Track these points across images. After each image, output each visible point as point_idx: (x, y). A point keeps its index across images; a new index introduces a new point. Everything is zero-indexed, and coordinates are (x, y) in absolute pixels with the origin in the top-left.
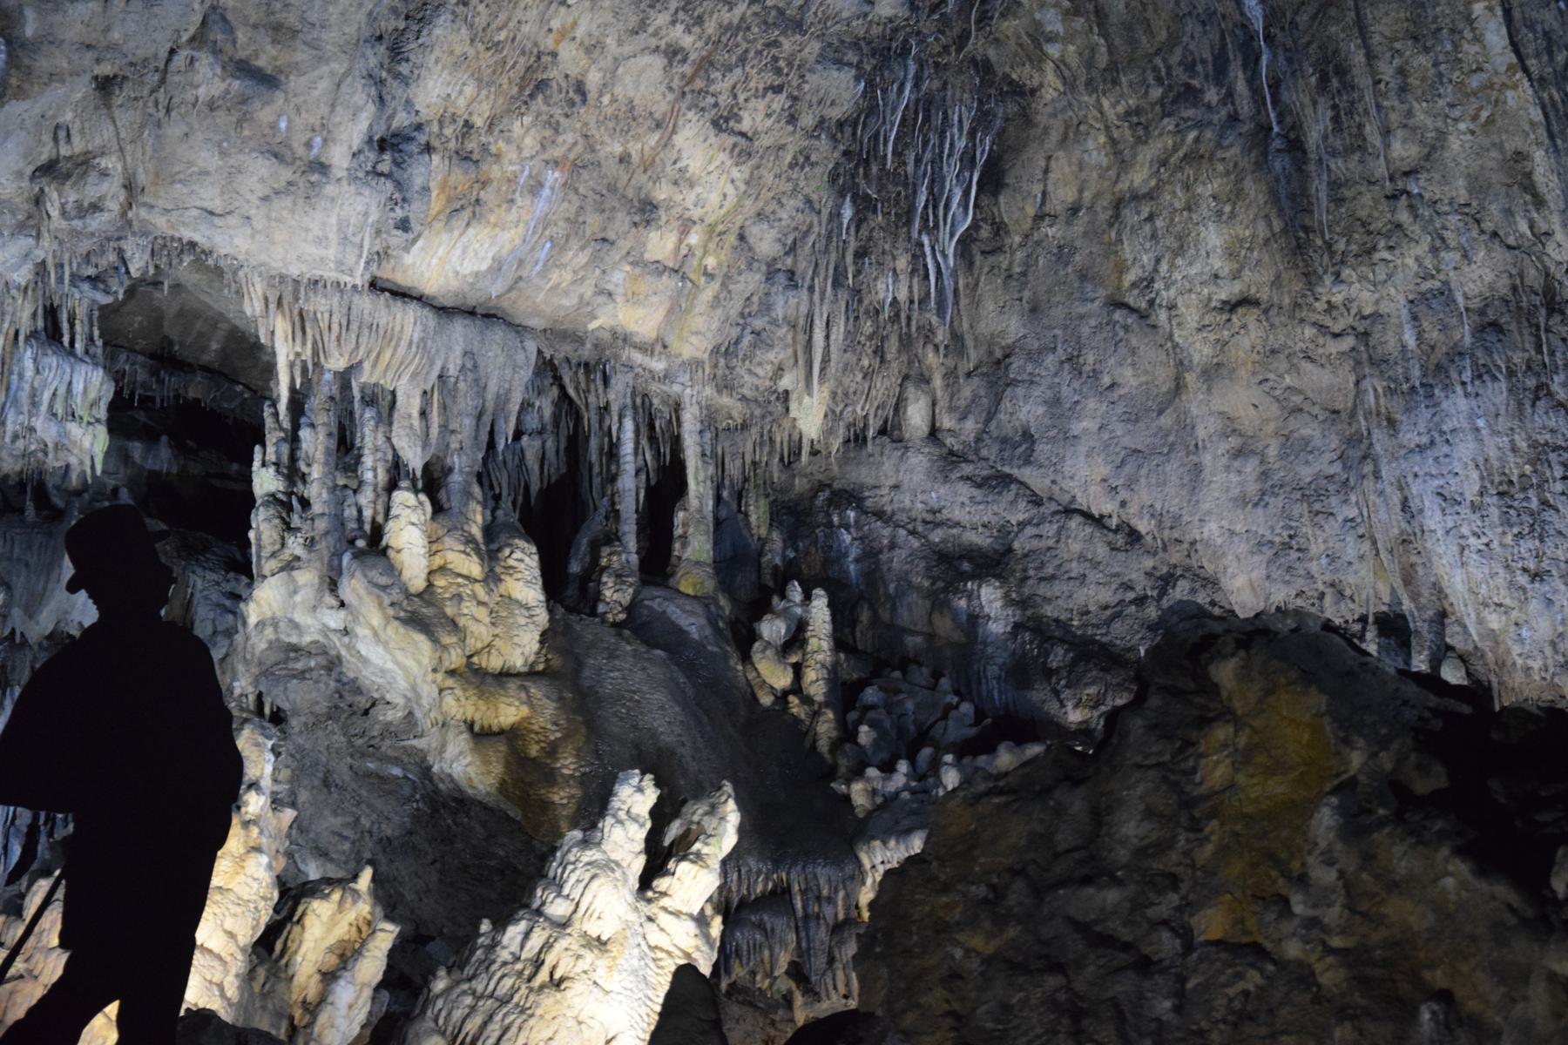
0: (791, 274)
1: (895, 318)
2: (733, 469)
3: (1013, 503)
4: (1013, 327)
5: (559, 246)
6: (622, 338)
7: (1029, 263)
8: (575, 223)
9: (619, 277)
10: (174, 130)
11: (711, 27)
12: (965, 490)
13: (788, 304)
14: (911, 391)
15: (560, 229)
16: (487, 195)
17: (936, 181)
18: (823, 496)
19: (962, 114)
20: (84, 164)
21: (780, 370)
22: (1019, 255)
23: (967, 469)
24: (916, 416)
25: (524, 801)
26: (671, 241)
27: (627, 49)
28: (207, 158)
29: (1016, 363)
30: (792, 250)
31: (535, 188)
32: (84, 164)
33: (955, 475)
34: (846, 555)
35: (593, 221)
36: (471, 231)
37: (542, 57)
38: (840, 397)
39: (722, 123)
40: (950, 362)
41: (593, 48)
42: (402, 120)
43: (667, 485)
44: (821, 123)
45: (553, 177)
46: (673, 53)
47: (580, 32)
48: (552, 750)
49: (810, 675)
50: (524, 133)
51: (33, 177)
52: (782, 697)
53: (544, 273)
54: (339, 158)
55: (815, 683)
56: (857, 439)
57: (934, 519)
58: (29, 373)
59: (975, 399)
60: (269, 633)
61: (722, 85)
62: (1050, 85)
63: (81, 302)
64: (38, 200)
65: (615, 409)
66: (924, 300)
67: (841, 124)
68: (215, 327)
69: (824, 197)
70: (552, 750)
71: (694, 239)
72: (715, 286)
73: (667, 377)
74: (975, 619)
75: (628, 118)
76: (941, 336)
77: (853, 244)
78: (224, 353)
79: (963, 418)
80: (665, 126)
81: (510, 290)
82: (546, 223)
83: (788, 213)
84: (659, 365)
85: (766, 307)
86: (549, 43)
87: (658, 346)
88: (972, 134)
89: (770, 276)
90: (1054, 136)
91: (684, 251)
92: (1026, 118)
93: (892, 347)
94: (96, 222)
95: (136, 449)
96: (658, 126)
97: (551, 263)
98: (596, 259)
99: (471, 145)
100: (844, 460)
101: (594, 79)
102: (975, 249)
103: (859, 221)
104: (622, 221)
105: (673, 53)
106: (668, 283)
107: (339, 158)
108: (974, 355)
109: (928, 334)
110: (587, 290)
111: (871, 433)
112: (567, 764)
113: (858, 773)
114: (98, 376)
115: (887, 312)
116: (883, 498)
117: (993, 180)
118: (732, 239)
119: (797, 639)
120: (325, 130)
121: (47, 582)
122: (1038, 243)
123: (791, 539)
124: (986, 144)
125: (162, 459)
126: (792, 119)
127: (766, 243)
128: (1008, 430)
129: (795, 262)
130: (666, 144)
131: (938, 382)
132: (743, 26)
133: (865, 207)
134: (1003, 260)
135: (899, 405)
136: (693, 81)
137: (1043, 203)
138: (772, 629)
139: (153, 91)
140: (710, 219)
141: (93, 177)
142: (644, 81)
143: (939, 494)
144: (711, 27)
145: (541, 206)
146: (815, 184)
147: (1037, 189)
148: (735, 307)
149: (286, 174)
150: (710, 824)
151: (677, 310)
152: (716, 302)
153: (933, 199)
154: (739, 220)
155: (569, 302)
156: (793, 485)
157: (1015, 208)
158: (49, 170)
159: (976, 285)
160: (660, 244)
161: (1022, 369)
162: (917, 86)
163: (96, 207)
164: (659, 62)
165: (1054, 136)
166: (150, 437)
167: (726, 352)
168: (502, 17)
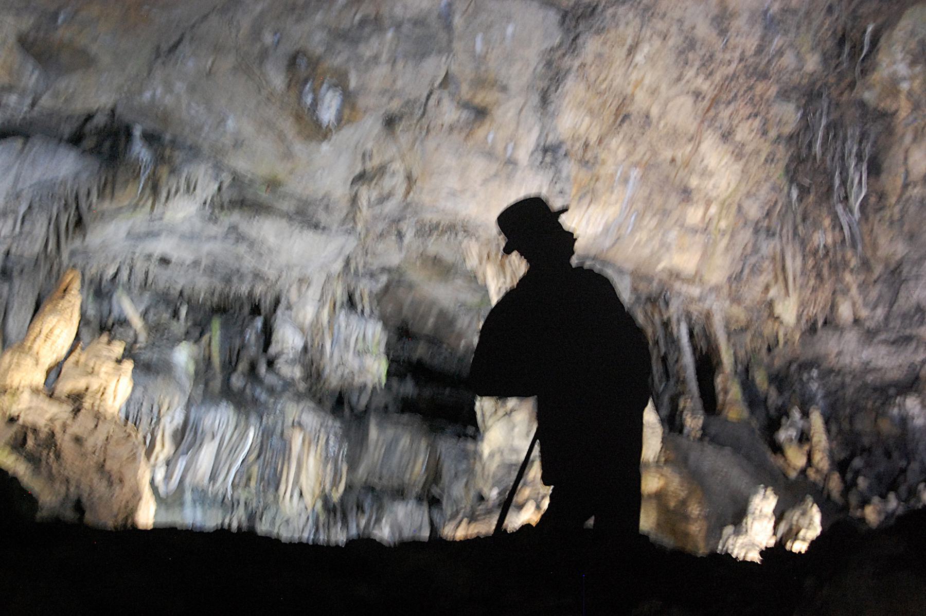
0: (768, 229)
1: (827, 254)
2: (741, 354)
3: (917, 348)
4: (900, 249)
5: (641, 216)
6: (676, 275)
7: (903, 213)
8: (648, 200)
9: (673, 235)
10: (431, 143)
11: (718, 77)
12: (883, 350)
13: (768, 247)
14: (839, 298)
15: (640, 205)
16: (599, 185)
17: (844, 171)
18: (794, 367)
19: (853, 132)
20: (382, 170)
21: (767, 288)
22: (897, 209)
23: (883, 336)
24: (845, 311)
25: (674, 532)
26: (700, 213)
27: (673, 92)
28: (449, 161)
29: (905, 270)
30: (768, 214)
31: (626, 181)
32: (382, 170)
33: (875, 340)
34: (815, 395)
35: (658, 201)
36: (592, 206)
37: (625, 100)
38: (803, 305)
39: (726, 136)
40: (862, 277)
41: (654, 92)
42: (551, 139)
43: (707, 364)
44: (779, 137)
45: (635, 173)
46: (697, 95)
47: (647, 81)
48: (684, 503)
49: (818, 457)
50: (617, 146)
51: (353, 182)
52: (803, 472)
53: (633, 232)
54: (523, 155)
55: (821, 460)
56: (812, 329)
57: (867, 368)
58: (343, 325)
59: (880, 296)
60: (497, 459)
61: (725, 113)
62: (904, 108)
63: (365, 288)
64: (354, 200)
65: (674, 320)
66: (843, 241)
67: (791, 137)
68: (430, 309)
69: (784, 183)
70: (684, 503)
71: (713, 210)
72: (727, 237)
73: (701, 299)
74: (904, 421)
75: (673, 136)
76: (854, 262)
77: (800, 211)
78: (436, 327)
79: (875, 307)
80: (695, 139)
81: (613, 245)
82: (632, 202)
83: (764, 192)
84: (695, 291)
85: (756, 250)
86: (629, 90)
87: (696, 278)
88: (860, 142)
89: (756, 231)
90: (908, 139)
91: (707, 220)
92: (890, 131)
93: (825, 272)
94: (391, 206)
95: (395, 383)
96: (690, 140)
97: (636, 228)
98: (660, 224)
99: (589, 155)
100: (803, 342)
101: (655, 111)
102: (869, 209)
103: (800, 199)
104: (674, 199)
105: (697, 95)
106: (699, 238)
107: (523, 155)
108: (878, 269)
109: (846, 263)
110: (656, 243)
111: (820, 324)
112: (694, 510)
113: (864, 502)
114: (379, 327)
115: (821, 252)
116: (832, 361)
117: (875, 168)
118: (734, 208)
119: (804, 438)
120: (513, 139)
121: (361, 451)
122: (907, 200)
123: (780, 391)
124: (868, 150)
125: (409, 388)
126: (765, 133)
127: (754, 211)
128: (905, 308)
129: (770, 221)
130: (696, 149)
131: (854, 291)
132: (734, 77)
133: (804, 192)
134: (887, 213)
135: (833, 307)
136: (710, 108)
137: (906, 177)
138: (785, 435)
139: (418, 121)
140: (722, 197)
141: (387, 178)
142: (682, 112)
143: (867, 354)
144: (718, 77)
145: (629, 192)
146: (777, 172)
147: (902, 170)
148: (738, 251)
149: (494, 167)
150: (804, 522)
151: (706, 255)
152: (727, 249)
153: (844, 183)
154: (737, 199)
155: (646, 252)
156: (773, 364)
157: (892, 182)
158: (361, 178)
159: (872, 231)
160: (694, 215)
161: (909, 272)
162: (828, 114)
163: (389, 196)
164: (688, 101)
165: (908, 139)
166: (402, 377)
167: (736, 278)
168: (602, 77)
